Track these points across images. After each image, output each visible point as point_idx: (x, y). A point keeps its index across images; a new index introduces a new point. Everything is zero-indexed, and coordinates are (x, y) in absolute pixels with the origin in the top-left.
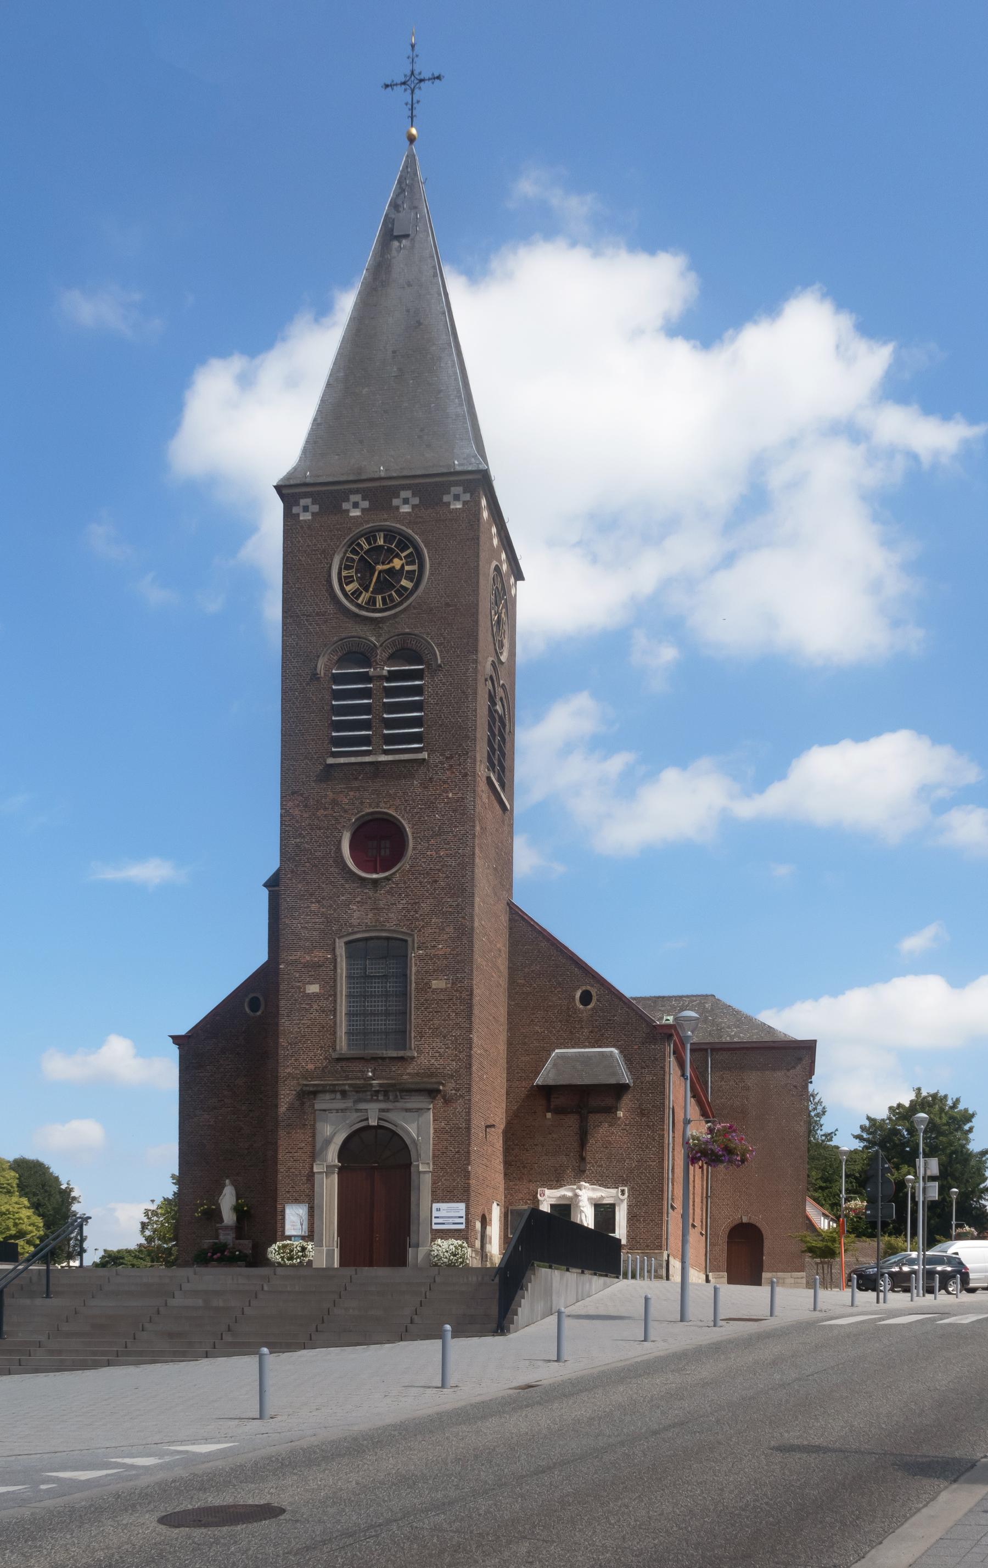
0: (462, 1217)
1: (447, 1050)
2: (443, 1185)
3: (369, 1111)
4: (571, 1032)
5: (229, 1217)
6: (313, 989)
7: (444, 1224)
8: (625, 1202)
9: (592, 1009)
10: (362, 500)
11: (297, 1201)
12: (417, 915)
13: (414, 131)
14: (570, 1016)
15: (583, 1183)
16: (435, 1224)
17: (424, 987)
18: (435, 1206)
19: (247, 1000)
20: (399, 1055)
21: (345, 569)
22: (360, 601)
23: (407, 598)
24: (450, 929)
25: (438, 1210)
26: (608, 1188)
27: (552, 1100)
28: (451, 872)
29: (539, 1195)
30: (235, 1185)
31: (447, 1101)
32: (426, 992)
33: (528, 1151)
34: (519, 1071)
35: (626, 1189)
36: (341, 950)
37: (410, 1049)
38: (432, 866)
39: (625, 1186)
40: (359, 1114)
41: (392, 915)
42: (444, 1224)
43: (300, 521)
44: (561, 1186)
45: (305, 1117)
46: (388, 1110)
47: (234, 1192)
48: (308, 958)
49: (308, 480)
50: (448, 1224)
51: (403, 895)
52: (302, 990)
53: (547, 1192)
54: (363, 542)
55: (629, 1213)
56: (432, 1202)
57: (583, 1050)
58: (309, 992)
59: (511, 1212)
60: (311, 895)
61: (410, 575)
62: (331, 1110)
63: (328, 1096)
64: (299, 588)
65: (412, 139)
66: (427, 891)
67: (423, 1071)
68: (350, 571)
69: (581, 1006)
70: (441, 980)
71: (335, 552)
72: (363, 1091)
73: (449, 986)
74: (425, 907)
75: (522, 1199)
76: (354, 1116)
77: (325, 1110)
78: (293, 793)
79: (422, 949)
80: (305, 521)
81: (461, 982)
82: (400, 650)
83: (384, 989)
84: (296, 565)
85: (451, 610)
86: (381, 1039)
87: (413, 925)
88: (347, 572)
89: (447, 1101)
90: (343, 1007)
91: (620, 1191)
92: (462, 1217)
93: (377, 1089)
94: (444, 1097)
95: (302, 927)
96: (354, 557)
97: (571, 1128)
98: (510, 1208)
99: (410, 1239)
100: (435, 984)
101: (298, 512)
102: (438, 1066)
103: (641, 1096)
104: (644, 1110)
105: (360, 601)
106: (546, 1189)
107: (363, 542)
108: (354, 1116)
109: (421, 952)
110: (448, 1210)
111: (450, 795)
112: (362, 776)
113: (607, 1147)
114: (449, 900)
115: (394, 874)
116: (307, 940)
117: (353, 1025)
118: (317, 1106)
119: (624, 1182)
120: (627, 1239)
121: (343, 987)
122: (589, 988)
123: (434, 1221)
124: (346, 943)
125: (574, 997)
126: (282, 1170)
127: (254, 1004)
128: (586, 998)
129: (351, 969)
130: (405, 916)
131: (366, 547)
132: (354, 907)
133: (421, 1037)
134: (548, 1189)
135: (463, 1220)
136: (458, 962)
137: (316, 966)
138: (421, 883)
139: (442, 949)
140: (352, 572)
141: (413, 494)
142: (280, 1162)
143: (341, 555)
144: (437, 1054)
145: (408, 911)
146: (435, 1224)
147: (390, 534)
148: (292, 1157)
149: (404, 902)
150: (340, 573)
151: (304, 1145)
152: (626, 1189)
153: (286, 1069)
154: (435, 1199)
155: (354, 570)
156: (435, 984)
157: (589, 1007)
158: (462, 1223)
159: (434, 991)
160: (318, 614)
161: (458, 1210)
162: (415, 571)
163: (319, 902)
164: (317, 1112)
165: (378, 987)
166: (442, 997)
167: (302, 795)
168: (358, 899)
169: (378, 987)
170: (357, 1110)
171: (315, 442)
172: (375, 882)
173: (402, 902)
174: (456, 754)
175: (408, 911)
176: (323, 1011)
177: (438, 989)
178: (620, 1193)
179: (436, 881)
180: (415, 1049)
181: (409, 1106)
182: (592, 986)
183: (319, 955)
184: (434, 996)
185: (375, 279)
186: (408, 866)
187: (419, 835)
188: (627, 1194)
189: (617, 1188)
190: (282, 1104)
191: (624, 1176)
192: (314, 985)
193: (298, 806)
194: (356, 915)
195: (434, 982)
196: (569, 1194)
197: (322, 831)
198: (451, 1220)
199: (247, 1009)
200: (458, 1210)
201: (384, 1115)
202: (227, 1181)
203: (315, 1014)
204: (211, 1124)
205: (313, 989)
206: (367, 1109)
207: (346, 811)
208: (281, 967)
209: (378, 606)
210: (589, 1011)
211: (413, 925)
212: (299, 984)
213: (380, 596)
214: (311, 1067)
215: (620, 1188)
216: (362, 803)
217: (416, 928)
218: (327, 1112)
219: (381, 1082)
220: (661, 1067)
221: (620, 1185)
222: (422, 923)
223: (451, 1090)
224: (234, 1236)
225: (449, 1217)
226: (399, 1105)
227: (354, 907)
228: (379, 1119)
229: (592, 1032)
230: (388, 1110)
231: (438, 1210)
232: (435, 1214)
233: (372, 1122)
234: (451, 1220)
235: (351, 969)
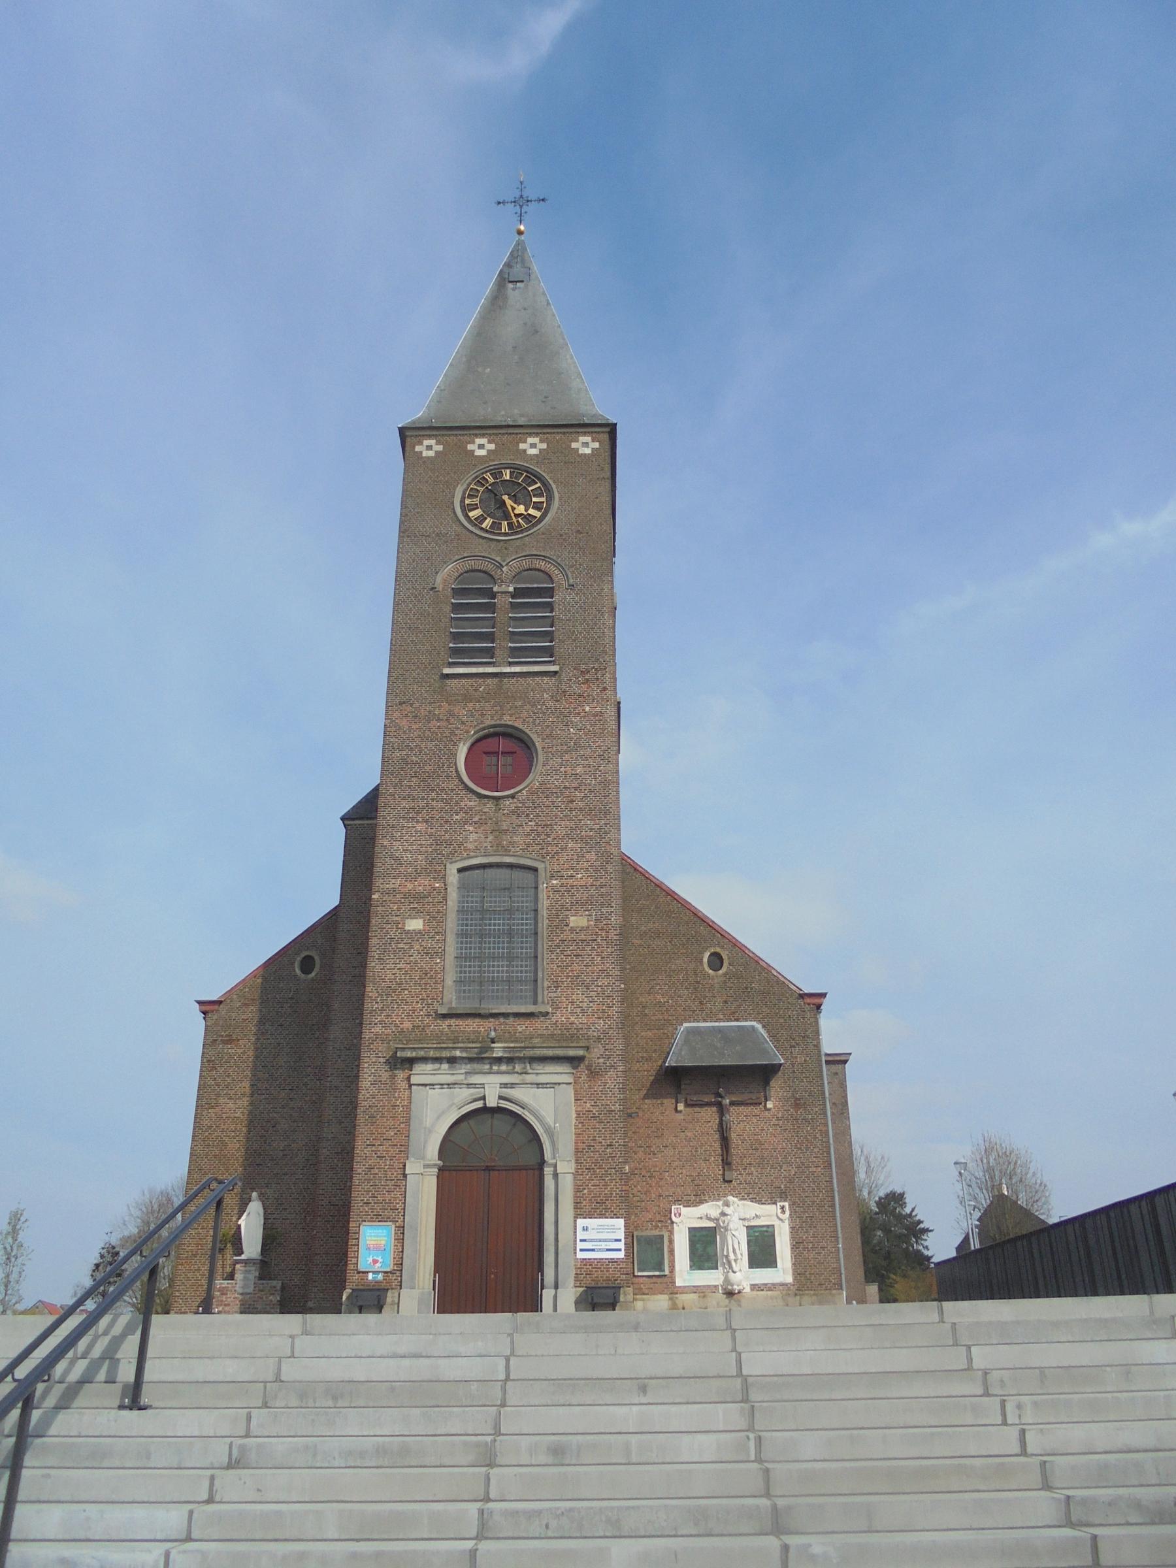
0: (620, 1240)
1: (591, 1004)
2: (590, 1192)
3: (486, 1086)
4: (701, 1003)
5: (252, 1246)
6: (415, 924)
7: (593, 1250)
8: (787, 1221)
9: (725, 974)
10: (488, 443)
11: (379, 1218)
12: (549, 839)
13: (522, 228)
14: (698, 982)
15: (730, 1198)
16: (581, 1250)
17: (559, 922)
18: (581, 1222)
19: (299, 959)
20: (528, 1011)
21: (468, 497)
22: (484, 526)
23: (534, 525)
24: (592, 856)
25: (585, 1229)
26: (763, 1204)
27: (683, 1087)
28: (590, 791)
29: (673, 1215)
30: (263, 1198)
31: (593, 1073)
32: (563, 931)
33: (654, 1154)
34: (640, 1050)
35: (786, 1204)
36: (453, 877)
37: (543, 1002)
38: (567, 784)
39: (785, 1201)
40: (472, 1091)
41: (517, 839)
42: (593, 1250)
43: (422, 457)
44: (701, 1202)
45: (396, 1095)
46: (512, 1085)
47: (261, 1211)
48: (410, 886)
49: (434, 425)
50: (600, 1250)
51: (532, 816)
52: (400, 926)
53: (684, 1211)
54: (488, 476)
55: (792, 1238)
56: (576, 1217)
57: (717, 1024)
58: (409, 928)
59: (638, 1240)
60: (418, 813)
61: (528, 518)
62: (433, 1085)
63: (429, 1067)
64: (418, 513)
65: (520, 233)
66: (562, 812)
67: (559, 1032)
68: (474, 500)
69: (710, 971)
70: (581, 916)
71: (458, 483)
72: (480, 1057)
73: (592, 923)
74: (560, 829)
75: (651, 1221)
76: (465, 1093)
77: (425, 1085)
78: (401, 704)
79: (556, 879)
80: (428, 458)
81: (607, 918)
82: (527, 570)
83: (506, 927)
84: (416, 492)
85: (583, 537)
86: (503, 990)
87: (545, 851)
88: (489, 479)
89: (593, 1073)
90: (451, 947)
91: (779, 1207)
92: (620, 1240)
93: (500, 1054)
94: (589, 1068)
95: (403, 850)
96: (478, 488)
97: (710, 1124)
98: (635, 1234)
99: (542, 1275)
100: (574, 921)
101: (421, 450)
102: (580, 1026)
103: (793, 1082)
104: (799, 1099)
105: (484, 526)
106: (681, 1207)
107: (488, 476)
108: (465, 1093)
109: (555, 882)
110: (600, 1229)
111: (587, 709)
112: (483, 687)
113: (756, 1149)
114: (589, 822)
115: (520, 791)
116: (410, 864)
117: (465, 972)
118: (414, 1080)
119: (783, 1196)
120: (793, 1274)
121: (452, 923)
122: (718, 950)
123: (580, 1245)
124: (460, 870)
125: (702, 959)
126: (360, 1171)
127: (307, 965)
128: (717, 961)
129: (463, 902)
130: (534, 840)
131: (491, 480)
132: (471, 829)
133: (557, 987)
134: (684, 1206)
135: (621, 1245)
136: (602, 895)
137: (417, 897)
138: (553, 802)
139: (581, 879)
140: (476, 501)
141: (540, 440)
142: (357, 1159)
143: (465, 486)
144: (579, 1010)
145: (539, 834)
146: (581, 1250)
147: (516, 469)
148: (376, 1152)
149: (533, 823)
150: (462, 501)
151: (392, 1134)
152: (786, 1204)
153: (373, 1029)
154: (580, 1212)
155: (478, 499)
156: (574, 921)
157: (721, 972)
158: (620, 1250)
159: (572, 930)
160: (438, 535)
161: (614, 1229)
162: (543, 502)
163: (426, 822)
164: (413, 1087)
165: (499, 925)
166: (583, 937)
167: (411, 705)
168: (476, 819)
169: (499, 925)
170: (469, 1085)
171: (439, 402)
172: (497, 799)
173: (530, 823)
174: (592, 669)
175: (539, 834)
176: (427, 953)
177: (578, 927)
178: (779, 1211)
179: (572, 801)
180: (548, 1003)
181: (542, 1079)
182: (722, 947)
183: (422, 884)
184: (572, 936)
185: (493, 304)
186: (537, 784)
187: (550, 750)
188: (788, 1213)
189: (775, 1203)
190: (366, 1076)
191: (782, 1186)
192: (415, 921)
193: (407, 715)
194: (473, 836)
195: (572, 918)
196: (714, 1213)
197: (434, 743)
198: (604, 1245)
199: (298, 971)
200: (614, 1229)
201: (515, 1093)
202: (254, 1194)
203: (416, 956)
204: (237, 1115)
205: (415, 924)
206: (484, 1084)
207: (463, 723)
208: (373, 897)
209: (503, 531)
210: (720, 976)
211: (545, 851)
212: (396, 918)
213: (506, 523)
214: (407, 1025)
215: (778, 1204)
216: (482, 715)
217: (548, 853)
218: (428, 1087)
219: (506, 1045)
220: (814, 1045)
221: (778, 1199)
222: (555, 849)
223: (598, 1058)
224: (257, 1274)
225: (600, 1240)
226: (529, 1078)
227: (471, 829)
228: (500, 1098)
229: (726, 1002)
230: (512, 1085)
231: (585, 1229)
232: (580, 1235)
233: (492, 1102)
234: (604, 1245)
235: (463, 902)
